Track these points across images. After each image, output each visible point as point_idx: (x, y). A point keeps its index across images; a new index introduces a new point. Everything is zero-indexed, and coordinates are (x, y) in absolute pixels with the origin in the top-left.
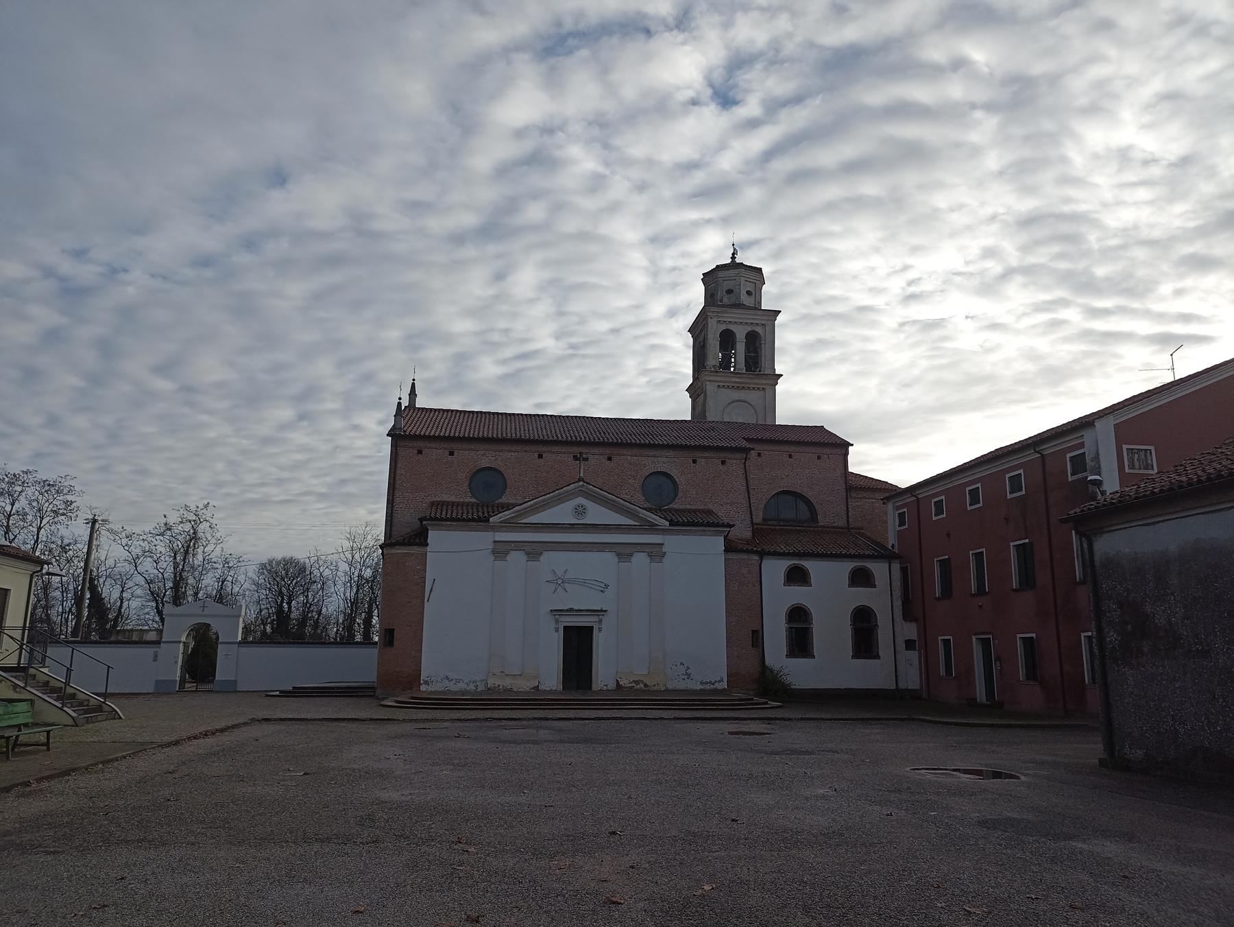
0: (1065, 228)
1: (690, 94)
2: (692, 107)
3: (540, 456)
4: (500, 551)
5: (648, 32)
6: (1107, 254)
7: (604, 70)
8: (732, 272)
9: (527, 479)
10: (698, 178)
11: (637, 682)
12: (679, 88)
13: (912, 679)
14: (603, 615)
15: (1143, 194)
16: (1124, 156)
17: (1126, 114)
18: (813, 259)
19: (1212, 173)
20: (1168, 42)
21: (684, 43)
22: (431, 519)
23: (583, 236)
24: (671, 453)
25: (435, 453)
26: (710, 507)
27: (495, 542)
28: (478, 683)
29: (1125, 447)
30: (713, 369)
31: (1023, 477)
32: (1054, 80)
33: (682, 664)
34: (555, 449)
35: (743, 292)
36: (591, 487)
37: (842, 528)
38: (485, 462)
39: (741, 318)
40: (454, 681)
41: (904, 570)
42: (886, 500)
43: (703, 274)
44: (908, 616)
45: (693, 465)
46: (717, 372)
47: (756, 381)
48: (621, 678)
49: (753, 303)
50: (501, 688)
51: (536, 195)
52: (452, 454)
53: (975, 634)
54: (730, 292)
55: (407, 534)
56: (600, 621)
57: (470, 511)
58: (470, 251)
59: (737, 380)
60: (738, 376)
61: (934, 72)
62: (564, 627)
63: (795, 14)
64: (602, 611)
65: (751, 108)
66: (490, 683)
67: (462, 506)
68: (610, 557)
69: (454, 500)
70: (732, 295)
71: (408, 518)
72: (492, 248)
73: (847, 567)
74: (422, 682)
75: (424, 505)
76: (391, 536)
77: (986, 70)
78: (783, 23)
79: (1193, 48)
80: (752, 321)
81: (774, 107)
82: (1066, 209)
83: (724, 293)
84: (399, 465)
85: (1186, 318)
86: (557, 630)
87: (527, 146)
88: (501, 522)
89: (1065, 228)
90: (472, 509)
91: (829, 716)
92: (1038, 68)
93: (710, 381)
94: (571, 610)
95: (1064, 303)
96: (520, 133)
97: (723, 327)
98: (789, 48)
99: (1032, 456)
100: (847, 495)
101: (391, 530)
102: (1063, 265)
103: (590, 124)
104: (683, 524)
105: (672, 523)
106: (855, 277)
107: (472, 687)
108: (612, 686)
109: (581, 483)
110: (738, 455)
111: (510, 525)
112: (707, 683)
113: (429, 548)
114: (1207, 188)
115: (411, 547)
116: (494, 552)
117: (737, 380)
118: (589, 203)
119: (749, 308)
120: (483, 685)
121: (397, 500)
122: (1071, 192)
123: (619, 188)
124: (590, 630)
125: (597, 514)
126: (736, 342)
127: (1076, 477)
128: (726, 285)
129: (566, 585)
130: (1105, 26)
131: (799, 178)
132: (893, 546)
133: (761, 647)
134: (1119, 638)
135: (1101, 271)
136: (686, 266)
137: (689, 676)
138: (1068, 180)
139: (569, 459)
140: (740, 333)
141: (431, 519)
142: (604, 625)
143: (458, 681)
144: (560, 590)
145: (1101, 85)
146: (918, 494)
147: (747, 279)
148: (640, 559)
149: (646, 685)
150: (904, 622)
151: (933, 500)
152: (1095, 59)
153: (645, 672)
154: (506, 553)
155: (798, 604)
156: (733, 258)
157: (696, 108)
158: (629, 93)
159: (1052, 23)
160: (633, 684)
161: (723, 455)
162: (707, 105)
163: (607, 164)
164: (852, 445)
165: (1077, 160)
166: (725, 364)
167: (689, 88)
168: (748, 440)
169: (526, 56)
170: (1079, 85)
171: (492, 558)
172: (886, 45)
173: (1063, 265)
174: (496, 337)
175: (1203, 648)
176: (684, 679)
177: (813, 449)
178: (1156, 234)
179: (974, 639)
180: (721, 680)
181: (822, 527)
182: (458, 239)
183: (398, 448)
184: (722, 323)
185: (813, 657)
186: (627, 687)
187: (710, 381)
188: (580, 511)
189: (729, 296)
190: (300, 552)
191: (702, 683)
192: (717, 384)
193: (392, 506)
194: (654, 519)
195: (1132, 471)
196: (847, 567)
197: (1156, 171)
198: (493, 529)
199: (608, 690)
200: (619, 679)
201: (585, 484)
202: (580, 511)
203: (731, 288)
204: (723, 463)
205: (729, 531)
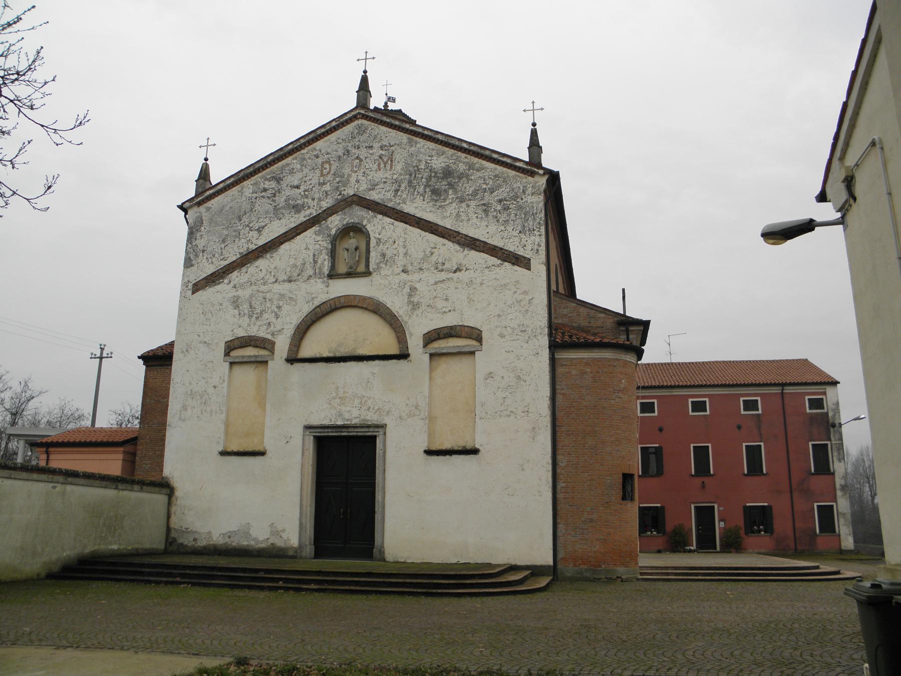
156: (386, 105)
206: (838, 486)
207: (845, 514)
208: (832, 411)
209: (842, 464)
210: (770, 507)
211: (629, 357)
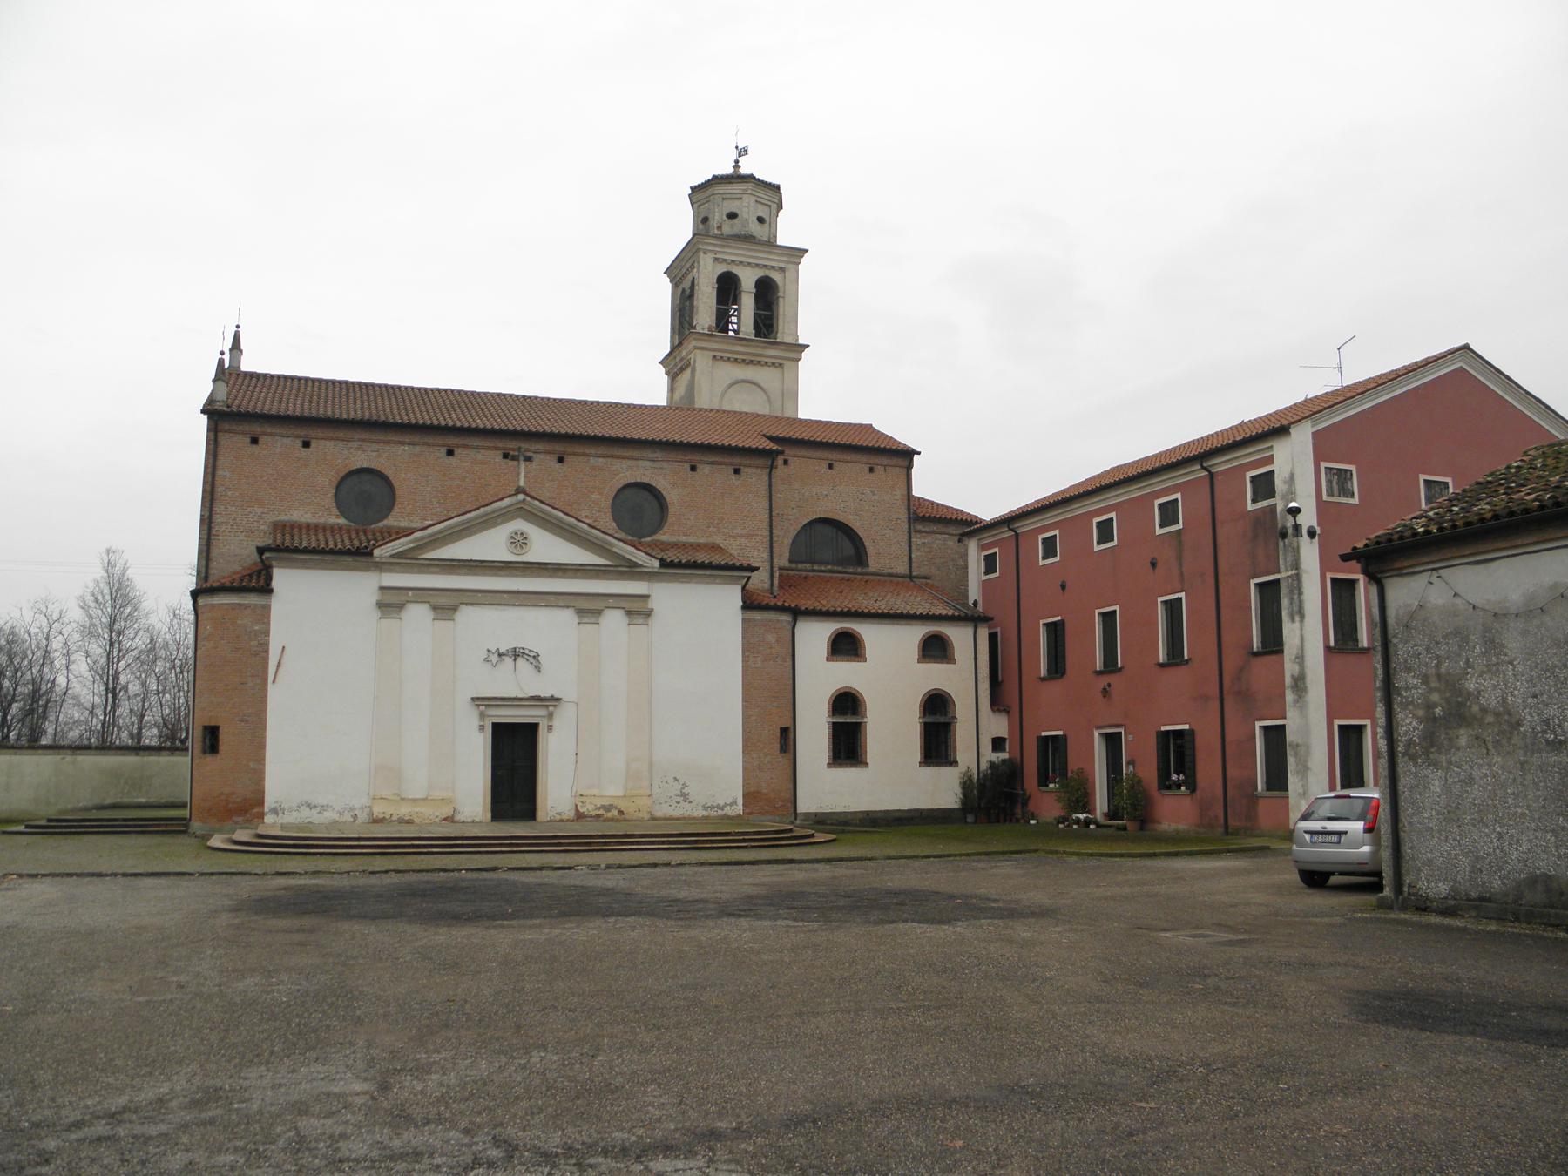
4: (391, 604)
8: (736, 188)
9: (429, 489)
11: (608, 808)
22: (277, 549)
25: (280, 446)
26: (718, 540)
27: (382, 588)
29: (1323, 465)
30: (706, 331)
31: (1180, 504)
33: (676, 779)
36: (537, 503)
37: (903, 577)
40: (318, 809)
41: (993, 638)
42: (963, 537)
43: (691, 188)
44: (997, 703)
46: (712, 335)
53: (1098, 727)
55: (235, 573)
56: (551, 716)
57: (338, 537)
64: (553, 699)
66: (378, 810)
67: (316, 530)
68: (566, 617)
69: (309, 521)
70: (736, 220)
71: (238, 552)
73: (916, 633)
75: (262, 527)
76: (206, 578)
83: (725, 217)
84: (219, 463)
86: (482, 728)
88: (392, 556)
90: (341, 536)
91: (1000, 848)
97: (722, 268)
99: (1195, 473)
100: (910, 528)
101: (207, 567)
104: (680, 565)
105: (664, 564)
108: (572, 815)
109: (521, 497)
110: (760, 462)
111: (407, 561)
112: (712, 807)
115: (247, 595)
116: (381, 605)
119: (760, 243)
121: (217, 518)
124: (533, 728)
125: (546, 547)
126: (740, 293)
127: (1260, 505)
132: (975, 603)
133: (792, 751)
134: (1421, 727)
137: (685, 797)
139: (499, 458)
140: (748, 279)
141: (277, 549)
142: (556, 723)
143: (324, 808)
146: (1018, 527)
147: (758, 199)
148: (614, 620)
149: (621, 812)
150: (991, 713)
151: (1041, 537)
153: (620, 793)
154: (401, 607)
155: (936, 689)
156: (737, 165)
161: (737, 460)
164: (919, 453)
166: (722, 322)
168: (771, 439)
171: (376, 614)
175: (1556, 738)
176: (678, 803)
177: (864, 458)
179: (1096, 734)
180: (734, 803)
184: (721, 263)
185: (866, 765)
186: (591, 816)
188: (519, 541)
190: (274, 594)
191: (705, 808)
193: (210, 529)
195: (1331, 499)
196: (916, 633)
198: (380, 567)
201: (528, 499)
202: (519, 541)
203: (735, 210)
204: (737, 471)
205: (749, 577)
206: (1288, 680)
207: (1298, 745)
208: (1282, 499)
209: (1297, 625)
210: (1192, 732)
211: (216, 599)
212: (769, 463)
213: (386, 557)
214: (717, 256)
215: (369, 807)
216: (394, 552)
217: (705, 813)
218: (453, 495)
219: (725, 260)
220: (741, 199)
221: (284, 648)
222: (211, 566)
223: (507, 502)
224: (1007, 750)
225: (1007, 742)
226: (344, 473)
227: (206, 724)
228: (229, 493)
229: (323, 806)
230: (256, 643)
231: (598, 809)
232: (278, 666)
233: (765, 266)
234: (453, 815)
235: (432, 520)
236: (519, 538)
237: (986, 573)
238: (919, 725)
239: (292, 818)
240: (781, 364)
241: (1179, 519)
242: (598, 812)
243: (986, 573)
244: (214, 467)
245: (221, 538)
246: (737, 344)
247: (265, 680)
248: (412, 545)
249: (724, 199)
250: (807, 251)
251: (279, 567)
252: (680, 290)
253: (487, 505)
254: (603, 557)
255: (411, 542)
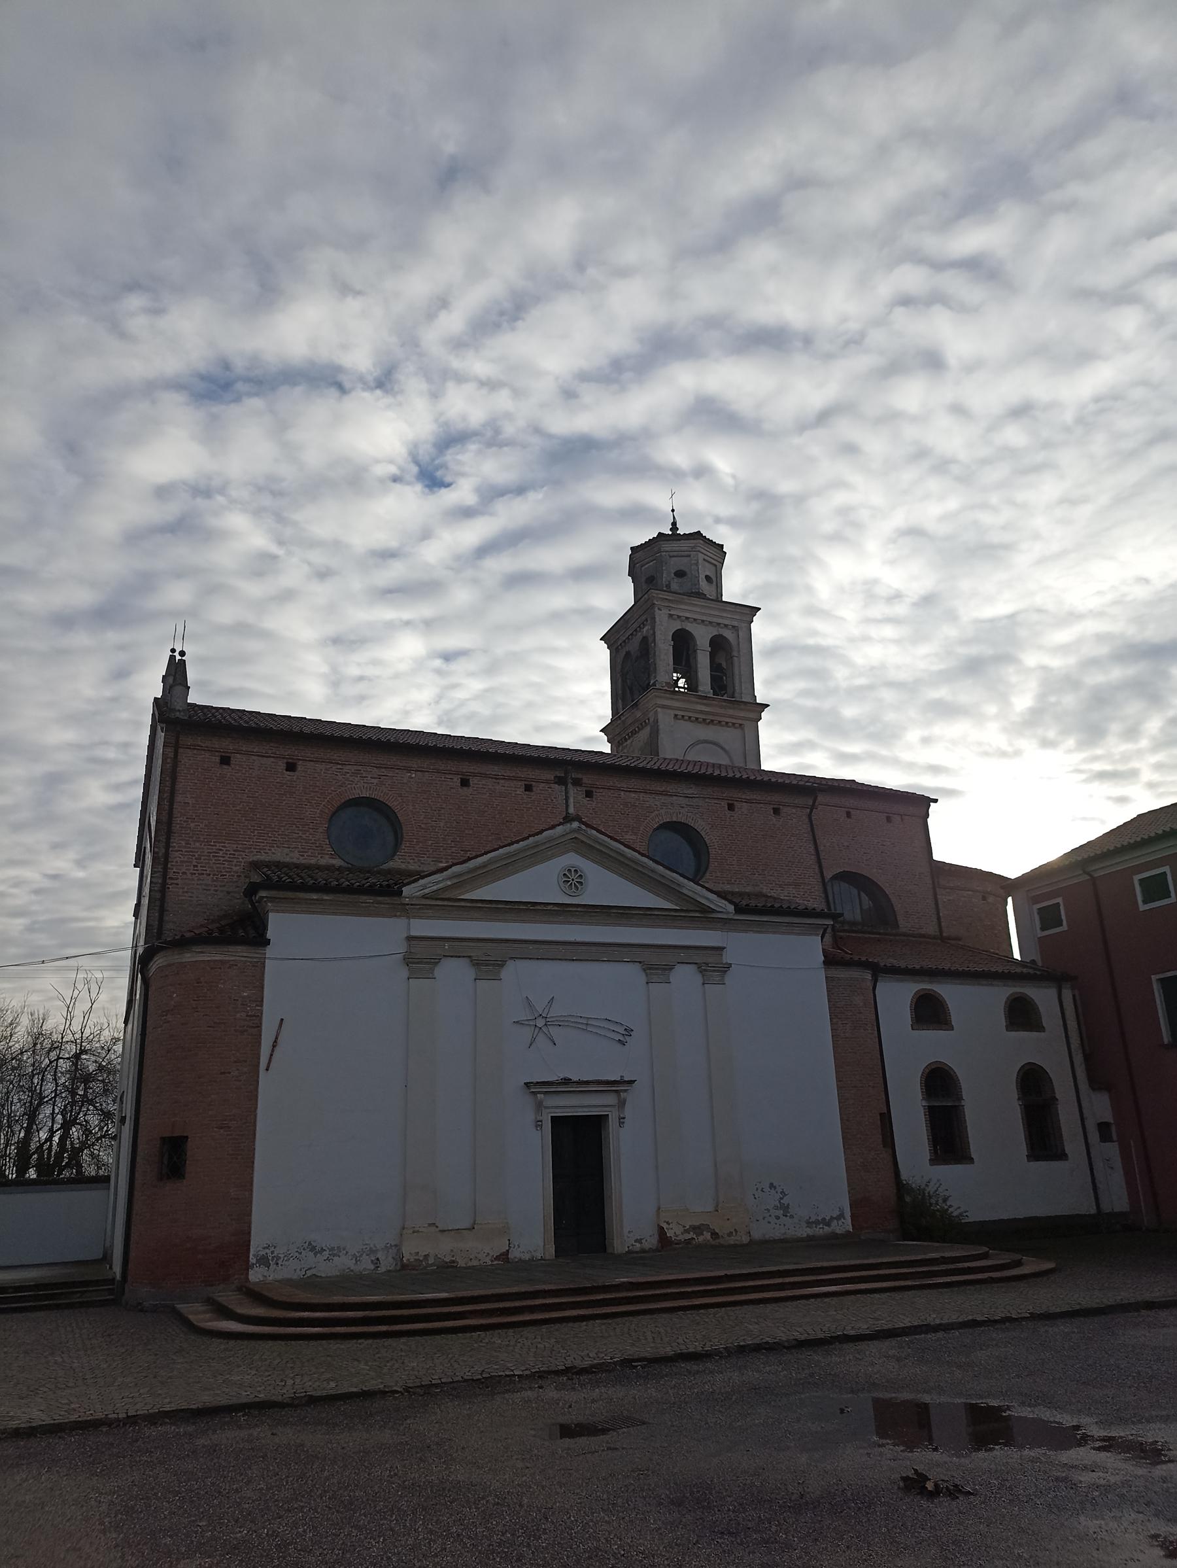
0: (810, 662)
1: (393, 469)
2: (393, 485)
3: (465, 783)
5: (342, 389)
6: (855, 693)
7: (281, 427)
10: (395, 572)
11: (698, 1229)
12: (377, 461)
13: (1117, 1199)
14: (625, 1091)
15: (889, 631)
16: (869, 591)
17: (872, 545)
18: (535, 678)
19: (951, 616)
20: (908, 475)
21: (389, 407)
23: (241, 629)
24: (692, 790)
27: (410, 939)
28: (379, 1255)
31: (1062, 908)
32: (800, 500)
33: (772, 1186)
34: (494, 769)
35: (702, 577)
36: (594, 832)
38: (360, 789)
39: (703, 614)
40: (326, 1254)
43: (632, 548)
45: (728, 813)
47: (731, 712)
48: (668, 1223)
49: (715, 595)
50: (431, 1261)
51: (180, 574)
52: (291, 767)
54: (680, 574)
56: (622, 1104)
58: (81, 639)
59: (704, 708)
60: (705, 701)
61: (673, 476)
62: (551, 1117)
63: (518, 393)
64: (631, 1081)
65: (463, 493)
66: (409, 1251)
72: (113, 637)
74: (252, 1260)
75: (235, 869)
77: (730, 481)
78: (503, 401)
79: (934, 484)
80: (720, 621)
81: (491, 495)
82: (811, 641)
84: (180, 786)
85: (935, 769)
86: (538, 1124)
87: (170, 511)
88: (424, 897)
89: (810, 662)
92: (787, 486)
93: (664, 707)
94: (566, 1081)
95: (809, 745)
96: (163, 492)
97: (677, 625)
98: (509, 430)
102: (809, 703)
103: (260, 489)
105: (739, 910)
106: (582, 702)
107: (366, 1265)
108: (651, 1242)
109: (575, 825)
112: (817, 1222)
113: (270, 951)
114: (950, 631)
115: (232, 948)
116: (409, 960)
117: (704, 708)
118: (254, 589)
120: (390, 1259)
121: (176, 857)
122: (819, 625)
123: (293, 575)
126: (695, 651)
128: (676, 564)
129: (553, 1031)
130: (850, 450)
131: (520, 580)
135: (850, 711)
136: (378, 677)
137: (785, 1208)
138: (812, 611)
140: (702, 637)
142: (628, 1112)
143: (335, 1252)
144: (541, 1039)
145: (844, 512)
147: (706, 558)
148: (685, 976)
149: (714, 1235)
152: (839, 484)
157: (397, 486)
158: (313, 458)
159: (797, 441)
160: (691, 1235)
161: (776, 798)
162: (409, 483)
163: (281, 543)
164: (936, 801)
165: (823, 590)
167: (391, 462)
169: (178, 397)
170: (823, 509)
171: (404, 972)
172: (622, 440)
173: (809, 703)
174: (111, 754)
176: (778, 1218)
178: (903, 676)
180: (841, 1216)
181: (905, 935)
182: (65, 621)
183: (181, 750)
185: (971, 1160)
186: (679, 1243)
187: (664, 707)
188: (573, 880)
189: (680, 580)
191: (809, 1223)
192: (672, 713)
194: (708, 899)
197: (901, 609)
198: (407, 911)
199: (643, 1251)
200: (665, 1226)
201: (583, 827)
202: (573, 880)
203: (682, 568)
204: (776, 811)
212: (811, 803)
213: (417, 897)
214: (672, 613)
215: (396, 1246)
216: (426, 891)
217: (810, 1231)
218: (471, 832)
219: (679, 617)
220: (689, 556)
221: (282, 1020)
222: (166, 918)
223: (559, 829)
224: (1115, 1137)
225: (1113, 1129)
226: (339, 804)
227: (167, 1135)
228: (192, 825)
229: (332, 1249)
230: (244, 1014)
231: (687, 1231)
232: (275, 1044)
233: (719, 624)
234: (508, 1251)
235: (447, 862)
236: (573, 876)
237: (1043, 929)
238: (1018, 1107)
239: (288, 1270)
240: (741, 725)
241: (1062, 921)
242: (688, 1236)
243: (1043, 929)
244: (173, 793)
245: (179, 881)
246: (697, 703)
247: (257, 1066)
248: (449, 883)
249: (670, 557)
250: (760, 609)
251: (278, 911)
252: (622, 653)
253: (537, 834)
254: (664, 898)
255: (449, 878)
